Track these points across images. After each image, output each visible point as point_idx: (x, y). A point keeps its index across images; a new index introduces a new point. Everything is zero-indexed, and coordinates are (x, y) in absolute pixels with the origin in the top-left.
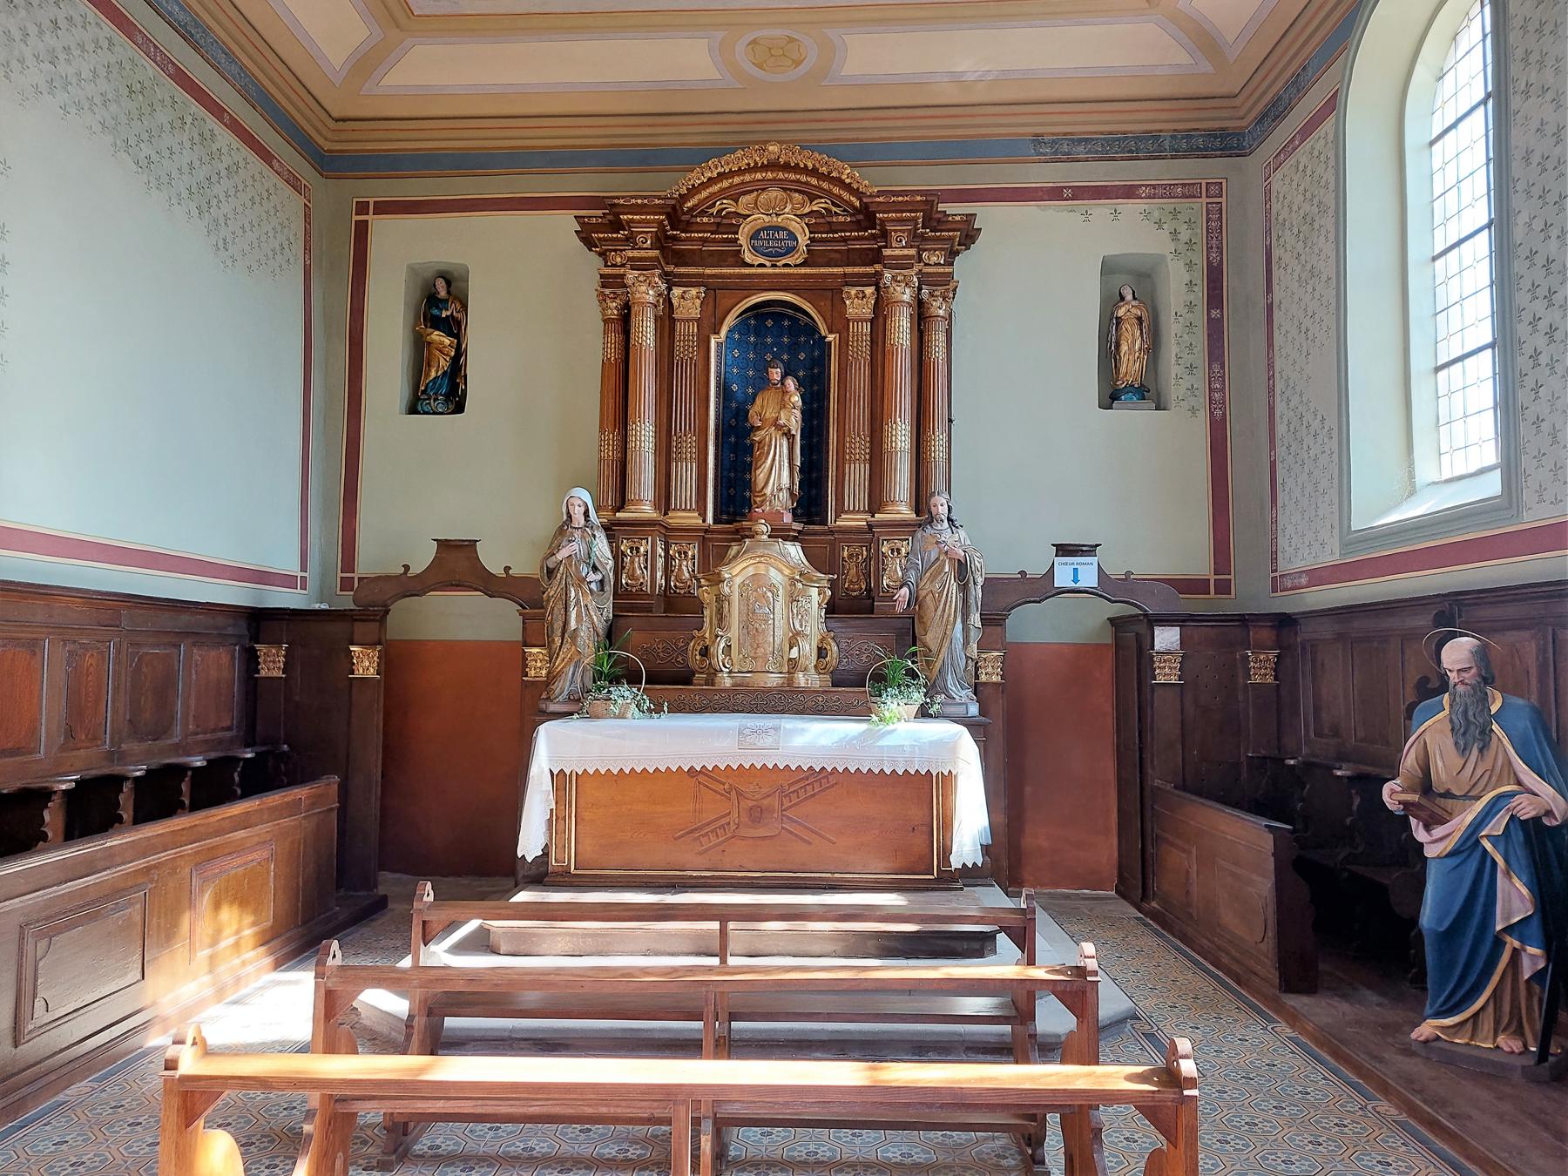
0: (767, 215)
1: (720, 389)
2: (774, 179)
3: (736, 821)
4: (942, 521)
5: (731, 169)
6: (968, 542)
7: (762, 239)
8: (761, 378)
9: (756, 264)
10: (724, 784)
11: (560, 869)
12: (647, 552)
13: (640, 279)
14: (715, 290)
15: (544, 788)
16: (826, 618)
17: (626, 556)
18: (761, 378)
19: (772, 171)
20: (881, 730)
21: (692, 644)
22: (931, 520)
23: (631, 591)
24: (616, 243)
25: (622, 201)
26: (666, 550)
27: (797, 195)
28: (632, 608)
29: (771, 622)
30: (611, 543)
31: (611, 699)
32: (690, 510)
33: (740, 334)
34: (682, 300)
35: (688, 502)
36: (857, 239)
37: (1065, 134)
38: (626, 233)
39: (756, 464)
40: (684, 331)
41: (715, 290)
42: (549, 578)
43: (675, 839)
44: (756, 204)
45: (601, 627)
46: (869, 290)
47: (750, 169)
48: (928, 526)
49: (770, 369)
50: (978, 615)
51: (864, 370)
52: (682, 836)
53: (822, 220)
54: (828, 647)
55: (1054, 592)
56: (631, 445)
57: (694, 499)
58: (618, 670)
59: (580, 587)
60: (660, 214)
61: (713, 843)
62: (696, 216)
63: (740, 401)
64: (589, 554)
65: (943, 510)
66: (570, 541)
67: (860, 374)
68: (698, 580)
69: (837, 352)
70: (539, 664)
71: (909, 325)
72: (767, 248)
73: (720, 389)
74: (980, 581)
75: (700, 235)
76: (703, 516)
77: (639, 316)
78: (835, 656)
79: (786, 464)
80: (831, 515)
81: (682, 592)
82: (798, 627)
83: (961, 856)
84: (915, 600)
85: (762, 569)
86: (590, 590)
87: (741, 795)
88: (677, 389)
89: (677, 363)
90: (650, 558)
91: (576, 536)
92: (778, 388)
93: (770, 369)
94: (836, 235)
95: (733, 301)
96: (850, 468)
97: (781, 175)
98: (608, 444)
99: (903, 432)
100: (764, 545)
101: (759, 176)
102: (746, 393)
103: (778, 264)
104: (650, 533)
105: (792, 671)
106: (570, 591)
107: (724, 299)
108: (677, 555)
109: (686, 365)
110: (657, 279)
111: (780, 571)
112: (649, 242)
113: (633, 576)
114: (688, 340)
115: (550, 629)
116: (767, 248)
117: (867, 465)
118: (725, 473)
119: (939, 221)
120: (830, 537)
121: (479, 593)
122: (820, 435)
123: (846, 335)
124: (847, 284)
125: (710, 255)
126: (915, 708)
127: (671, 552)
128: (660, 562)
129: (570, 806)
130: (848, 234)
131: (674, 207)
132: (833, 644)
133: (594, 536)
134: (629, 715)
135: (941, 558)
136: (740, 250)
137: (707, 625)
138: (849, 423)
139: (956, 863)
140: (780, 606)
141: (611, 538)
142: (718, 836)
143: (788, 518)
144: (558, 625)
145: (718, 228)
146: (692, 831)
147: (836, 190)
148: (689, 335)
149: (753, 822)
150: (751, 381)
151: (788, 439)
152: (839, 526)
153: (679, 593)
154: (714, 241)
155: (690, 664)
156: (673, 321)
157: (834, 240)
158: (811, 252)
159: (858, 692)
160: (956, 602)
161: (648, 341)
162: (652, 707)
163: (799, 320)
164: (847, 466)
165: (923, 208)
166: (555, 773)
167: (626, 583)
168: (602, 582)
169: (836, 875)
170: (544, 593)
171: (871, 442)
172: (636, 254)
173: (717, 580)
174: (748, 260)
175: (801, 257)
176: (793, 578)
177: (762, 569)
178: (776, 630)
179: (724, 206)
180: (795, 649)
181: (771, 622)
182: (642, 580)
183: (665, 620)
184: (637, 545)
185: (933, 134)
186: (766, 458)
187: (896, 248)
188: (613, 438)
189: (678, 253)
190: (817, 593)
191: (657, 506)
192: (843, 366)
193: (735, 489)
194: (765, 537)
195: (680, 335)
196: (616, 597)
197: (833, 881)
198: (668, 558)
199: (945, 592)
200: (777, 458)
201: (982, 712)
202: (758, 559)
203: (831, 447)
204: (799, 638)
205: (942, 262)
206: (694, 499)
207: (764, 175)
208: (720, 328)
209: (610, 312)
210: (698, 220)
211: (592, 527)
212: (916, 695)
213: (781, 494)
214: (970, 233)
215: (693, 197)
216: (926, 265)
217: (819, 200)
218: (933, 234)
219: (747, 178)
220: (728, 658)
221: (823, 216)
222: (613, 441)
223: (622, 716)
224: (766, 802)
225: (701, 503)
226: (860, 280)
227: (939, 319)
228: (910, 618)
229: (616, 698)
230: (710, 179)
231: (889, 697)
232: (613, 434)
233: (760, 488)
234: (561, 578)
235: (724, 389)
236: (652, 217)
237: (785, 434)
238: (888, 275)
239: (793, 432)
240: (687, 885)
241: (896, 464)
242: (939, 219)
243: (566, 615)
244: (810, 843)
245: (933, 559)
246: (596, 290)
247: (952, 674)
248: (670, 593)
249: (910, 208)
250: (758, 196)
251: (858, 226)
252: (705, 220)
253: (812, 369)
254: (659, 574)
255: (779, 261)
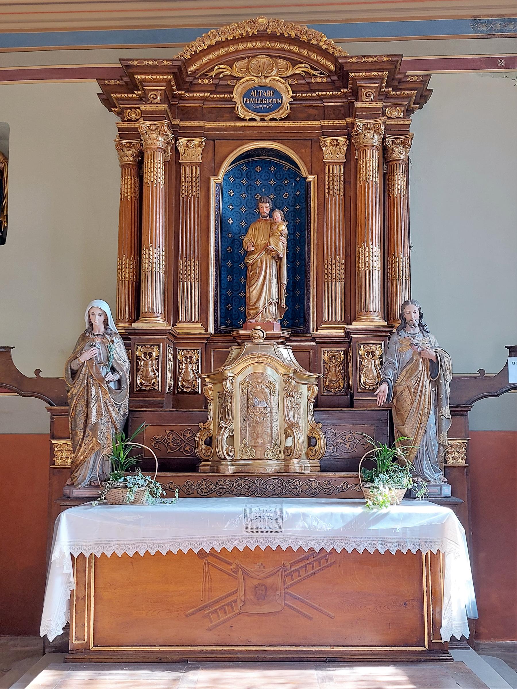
0: (257, 77)
1: (218, 222)
2: (263, 48)
3: (243, 599)
4: (415, 326)
5: (227, 39)
6: (437, 344)
7: (252, 97)
8: (252, 214)
9: (248, 118)
10: (230, 564)
11: (80, 647)
12: (159, 356)
13: (151, 128)
14: (214, 140)
15: (65, 571)
16: (314, 411)
17: (140, 360)
18: (252, 214)
19: (261, 41)
20: (375, 513)
21: (198, 435)
22: (404, 325)
23: (145, 390)
24: (131, 102)
25: (136, 63)
26: (175, 355)
27: (281, 61)
28: (147, 405)
29: (268, 414)
30: (128, 349)
31: (127, 487)
32: (194, 322)
33: (235, 177)
34: (186, 148)
35: (193, 315)
36: (331, 97)
37: (498, 16)
38: (140, 93)
39: (250, 281)
40: (189, 174)
41: (214, 140)
42: (73, 378)
43: (187, 616)
44: (247, 68)
45: (119, 421)
46: (342, 140)
47: (243, 39)
48: (402, 331)
49: (260, 204)
50: (448, 407)
51: (339, 205)
52: (192, 614)
53: (303, 82)
54: (317, 437)
55: (509, 387)
56: (144, 266)
57: (197, 313)
58: (133, 460)
59: (100, 386)
60: (168, 73)
61: (221, 619)
62: (198, 78)
63: (235, 232)
64: (108, 358)
65: (416, 316)
66: (91, 346)
67: (335, 207)
68: (203, 379)
69: (316, 190)
70: (65, 454)
71: (377, 165)
72: (257, 105)
73: (218, 222)
74: (449, 378)
75: (201, 95)
76: (205, 325)
77: (151, 159)
78: (323, 444)
79: (275, 283)
80: (313, 324)
81: (188, 390)
82: (292, 419)
83: (451, 630)
84: (393, 394)
85: (260, 368)
86: (109, 388)
87: (248, 575)
88: (183, 222)
89: (183, 200)
90: (161, 361)
91: (97, 342)
92: (267, 220)
93: (260, 204)
94: (314, 95)
95: (230, 148)
96: (328, 286)
97: (268, 44)
98: (125, 268)
99: (375, 253)
100: (261, 347)
101: (250, 45)
102: (239, 226)
103: (266, 118)
104: (161, 340)
105: (288, 458)
106: (91, 390)
107: (222, 147)
108: (184, 360)
109: (190, 202)
110: (166, 129)
111: (276, 370)
112: (159, 98)
113: (146, 377)
114: (192, 181)
115: (73, 424)
116: (257, 105)
117: (343, 283)
118: (224, 292)
119: (400, 81)
120: (312, 343)
121: (15, 394)
122: (302, 259)
123: (323, 176)
124: (323, 134)
125: (209, 112)
126: (403, 492)
127: (179, 357)
128: (170, 365)
129: (90, 587)
130: (324, 93)
131: (179, 68)
132: (321, 433)
133: (113, 341)
134: (144, 501)
135: (415, 358)
136: (234, 108)
137: (211, 417)
138: (327, 248)
139: (446, 637)
140: (277, 401)
141: (128, 346)
142: (225, 613)
143: (277, 327)
144: (80, 420)
145: (216, 88)
146: (202, 609)
147: (314, 56)
148: (192, 177)
149: (258, 599)
150: (244, 216)
151: (276, 262)
152: (321, 334)
153: (186, 392)
154: (213, 100)
155: (197, 453)
156: (179, 165)
157: (312, 99)
158: (293, 109)
159: (347, 477)
160: (430, 396)
161: (159, 179)
162: (165, 494)
163: (284, 166)
164: (326, 284)
165: (388, 67)
166: (76, 556)
167: (140, 383)
168: (119, 381)
169: (336, 648)
170: (68, 392)
171: (346, 264)
172: (148, 107)
173: (221, 379)
174: (241, 115)
175: (286, 112)
176: (288, 376)
177: (260, 368)
178: (273, 422)
179: (221, 70)
180: (290, 439)
181: (268, 414)
182: (154, 380)
183: (175, 414)
184: (150, 350)
185: (390, 16)
186: (259, 277)
187: (365, 101)
188: (129, 262)
189: (182, 110)
190: (306, 389)
191: (167, 318)
192: (321, 201)
193: (232, 304)
194: (261, 341)
195: (185, 177)
196: (132, 395)
197: (333, 654)
198: (176, 362)
199: (420, 388)
200: (268, 277)
201: (453, 493)
202: (257, 359)
203: (312, 269)
204: (293, 429)
205: (402, 116)
206: (197, 313)
207: (254, 44)
208: (219, 171)
209: (126, 158)
210: (200, 81)
211: (111, 334)
212: (405, 481)
213: (271, 308)
214: (424, 94)
215: (195, 62)
216: (389, 118)
217: (300, 65)
218: (394, 93)
219: (240, 46)
220: (231, 447)
221: (303, 78)
222: (129, 265)
223: (136, 502)
224: (269, 581)
225: (203, 316)
226: (335, 132)
227: (400, 162)
228: (387, 410)
229: (132, 486)
230: (209, 47)
231: (381, 483)
232: (130, 259)
233: (254, 302)
234: (84, 378)
235: (222, 222)
236: (161, 77)
237: (274, 258)
238: (359, 123)
239: (281, 256)
240: (198, 660)
241: (369, 281)
242: (401, 79)
243: (87, 411)
244: (310, 618)
245: (408, 359)
246: (115, 141)
247: (426, 459)
248: (178, 391)
249: (378, 67)
250: (249, 62)
251: (333, 86)
252: (206, 81)
253: (294, 205)
254: (169, 375)
255: (267, 116)
